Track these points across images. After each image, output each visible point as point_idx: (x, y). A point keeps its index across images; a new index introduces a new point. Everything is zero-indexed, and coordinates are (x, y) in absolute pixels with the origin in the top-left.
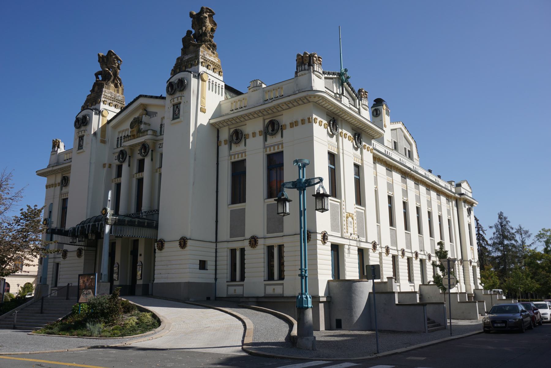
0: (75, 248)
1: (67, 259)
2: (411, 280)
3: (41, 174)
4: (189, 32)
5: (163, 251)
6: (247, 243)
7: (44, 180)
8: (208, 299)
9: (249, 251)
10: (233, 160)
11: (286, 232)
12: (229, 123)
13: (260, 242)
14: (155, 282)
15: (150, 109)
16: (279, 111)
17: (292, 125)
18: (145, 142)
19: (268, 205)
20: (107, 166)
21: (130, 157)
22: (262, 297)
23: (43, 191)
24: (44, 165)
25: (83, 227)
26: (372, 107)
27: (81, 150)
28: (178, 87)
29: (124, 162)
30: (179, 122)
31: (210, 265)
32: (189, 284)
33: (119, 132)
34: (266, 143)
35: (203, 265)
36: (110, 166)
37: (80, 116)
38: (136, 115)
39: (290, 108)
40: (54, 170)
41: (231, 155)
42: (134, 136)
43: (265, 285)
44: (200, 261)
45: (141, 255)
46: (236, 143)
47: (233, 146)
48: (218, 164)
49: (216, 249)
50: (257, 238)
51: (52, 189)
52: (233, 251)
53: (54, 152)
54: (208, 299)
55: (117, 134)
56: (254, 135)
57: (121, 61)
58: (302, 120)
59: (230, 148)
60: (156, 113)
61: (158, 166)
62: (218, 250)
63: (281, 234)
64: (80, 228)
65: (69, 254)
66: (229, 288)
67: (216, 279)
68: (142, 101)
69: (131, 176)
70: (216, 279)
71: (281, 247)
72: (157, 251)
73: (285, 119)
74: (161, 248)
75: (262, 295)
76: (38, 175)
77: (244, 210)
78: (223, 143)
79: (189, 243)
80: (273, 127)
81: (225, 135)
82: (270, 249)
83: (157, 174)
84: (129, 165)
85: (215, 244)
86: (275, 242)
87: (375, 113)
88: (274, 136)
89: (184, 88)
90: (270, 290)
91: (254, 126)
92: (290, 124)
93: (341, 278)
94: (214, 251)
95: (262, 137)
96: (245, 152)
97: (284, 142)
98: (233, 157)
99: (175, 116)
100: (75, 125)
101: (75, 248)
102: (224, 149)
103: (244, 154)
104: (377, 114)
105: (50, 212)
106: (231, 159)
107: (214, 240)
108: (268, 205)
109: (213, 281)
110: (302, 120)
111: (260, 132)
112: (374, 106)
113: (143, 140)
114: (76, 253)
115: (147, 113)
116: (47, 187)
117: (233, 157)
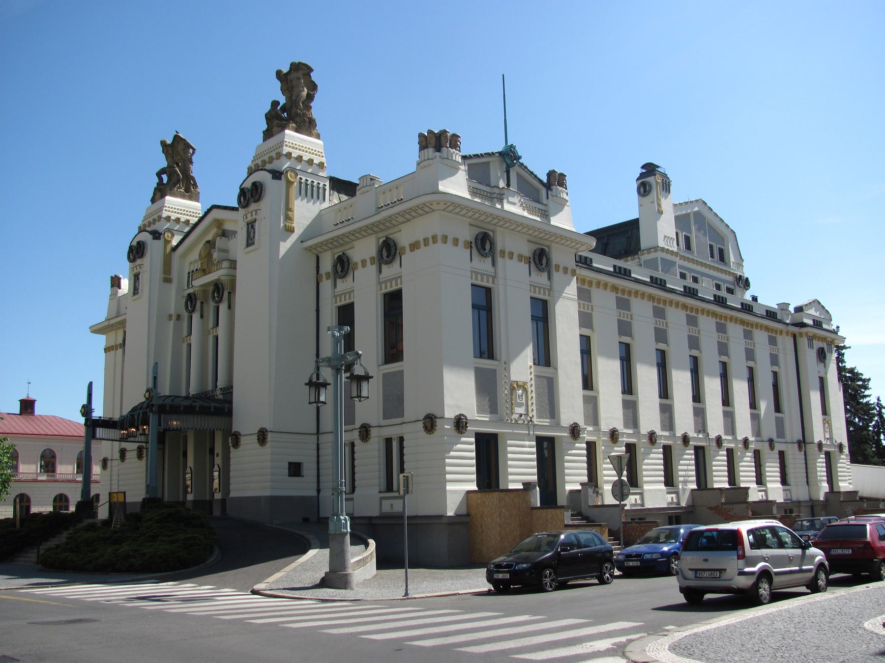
0: (136, 445)
1: (126, 461)
2: (669, 481)
3: (97, 330)
4: (275, 104)
5: (241, 448)
6: (356, 434)
7: (101, 341)
8: (306, 520)
9: (359, 446)
10: (339, 304)
11: (406, 418)
12: (376, 229)
13: (374, 432)
14: (232, 495)
15: (228, 227)
16: (395, 226)
17: (414, 246)
18: (218, 280)
19: (384, 375)
20: (174, 318)
21: (202, 303)
22: (376, 517)
23: (100, 358)
24: (100, 315)
25: (132, 416)
26: (638, 179)
27: (136, 297)
28: (252, 196)
29: (220, 301)
30: (255, 250)
31: (309, 469)
32: (273, 500)
33: (191, 263)
34: (381, 276)
35: (295, 469)
36: (179, 317)
37: (248, 185)
38: (209, 237)
39: (408, 220)
40: (112, 325)
41: (336, 297)
42: (204, 270)
43: (382, 498)
44: (290, 463)
45: (218, 455)
46: (387, 263)
47: (339, 281)
48: (318, 311)
49: (318, 445)
50: (370, 427)
51: (112, 353)
52: (388, 441)
53: (114, 295)
54: (306, 520)
55: (187, 265)
56: (364, 263)
57: (194, 150)
58: (362, 261)
59: (335, 285)
60: (236, 232)
61: (185, 333)
62: (320, 446)
63: (399, 420)
64: (141, 415)
65: (128, 455)
66: (384, 502)
67: (319, 491)
68: (215, 214)
69: (205, 333)
70: (319, 491)
71: (401, 439)
72: (232, 449)
73: (404, 237)
74: (236, 444)
75: (375, 513)
76: (93, 332)
77: (401, 373)
78: (324, 276)
79: (270, 436)
80: (389, 251)
81: (327, 265)
82: (388, 441)
83: (185, 346)
84: (202, 316)
85: (316, 437)
86: (393, 432)
87: (642, 190)
88: (390, 265)
89: (260, 196)
90: (387, 507)
91: (364, 250)
92: (410, 245)
93: (501, 488)
94: (315, 446)
95: (374, 266)
96: (400, 277)
97: (403, 274)
98: (383, 285)
99: (250, 242)
100: (129, 258)
101: (136, 445)
102: (326, 285)
103: (399, 280)
104: (645, 191)
105: (155, 378)
106: (381, 289)
107: (315, 431)
108: (384, 375)
109: (315, 493)
110: (362, 261)
111: (371, 259)
112: (642, 176)
113: (216, 277)
114: (256, 437)
115: (224, 234)
116: (107, 350)
117: (383, 285)
